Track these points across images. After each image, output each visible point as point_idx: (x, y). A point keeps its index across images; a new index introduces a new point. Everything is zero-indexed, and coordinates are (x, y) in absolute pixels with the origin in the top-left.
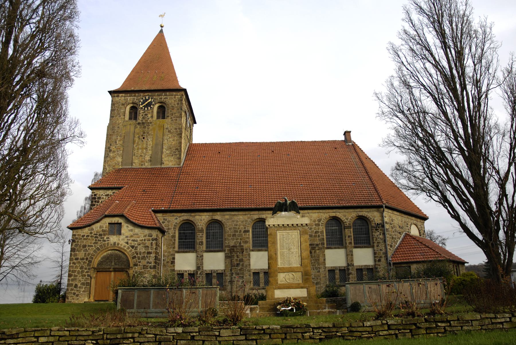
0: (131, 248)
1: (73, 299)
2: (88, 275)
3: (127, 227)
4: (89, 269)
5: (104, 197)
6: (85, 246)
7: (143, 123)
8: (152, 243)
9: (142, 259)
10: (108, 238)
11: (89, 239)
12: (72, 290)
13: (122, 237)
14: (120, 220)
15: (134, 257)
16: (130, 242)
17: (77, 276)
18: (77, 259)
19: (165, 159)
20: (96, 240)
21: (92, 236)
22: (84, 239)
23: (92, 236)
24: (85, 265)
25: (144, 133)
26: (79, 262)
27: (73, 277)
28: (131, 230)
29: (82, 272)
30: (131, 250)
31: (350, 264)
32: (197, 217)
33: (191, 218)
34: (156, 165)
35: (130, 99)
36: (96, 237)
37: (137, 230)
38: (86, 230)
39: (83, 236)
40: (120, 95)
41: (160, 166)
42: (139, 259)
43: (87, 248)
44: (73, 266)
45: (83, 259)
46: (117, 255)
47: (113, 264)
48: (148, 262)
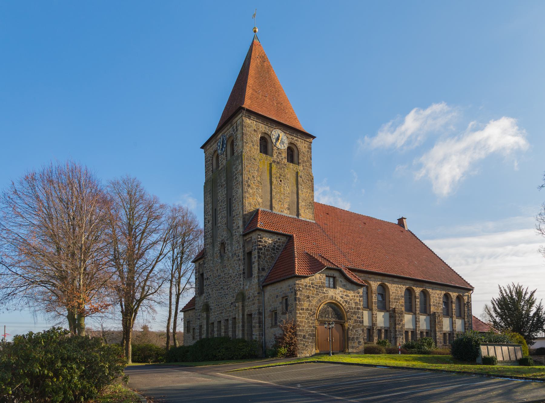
2: (313, 326)
3: (341, 281)
7: (278, 163)
14: (336, 274)
18: (302, 309)
20: (317, 291)
21: (313, 287)
22: (307, 289)
29: (309, 322)
35: (263, 128)
39: (306, 286)
45: (307, 309)
48: (358, 317)
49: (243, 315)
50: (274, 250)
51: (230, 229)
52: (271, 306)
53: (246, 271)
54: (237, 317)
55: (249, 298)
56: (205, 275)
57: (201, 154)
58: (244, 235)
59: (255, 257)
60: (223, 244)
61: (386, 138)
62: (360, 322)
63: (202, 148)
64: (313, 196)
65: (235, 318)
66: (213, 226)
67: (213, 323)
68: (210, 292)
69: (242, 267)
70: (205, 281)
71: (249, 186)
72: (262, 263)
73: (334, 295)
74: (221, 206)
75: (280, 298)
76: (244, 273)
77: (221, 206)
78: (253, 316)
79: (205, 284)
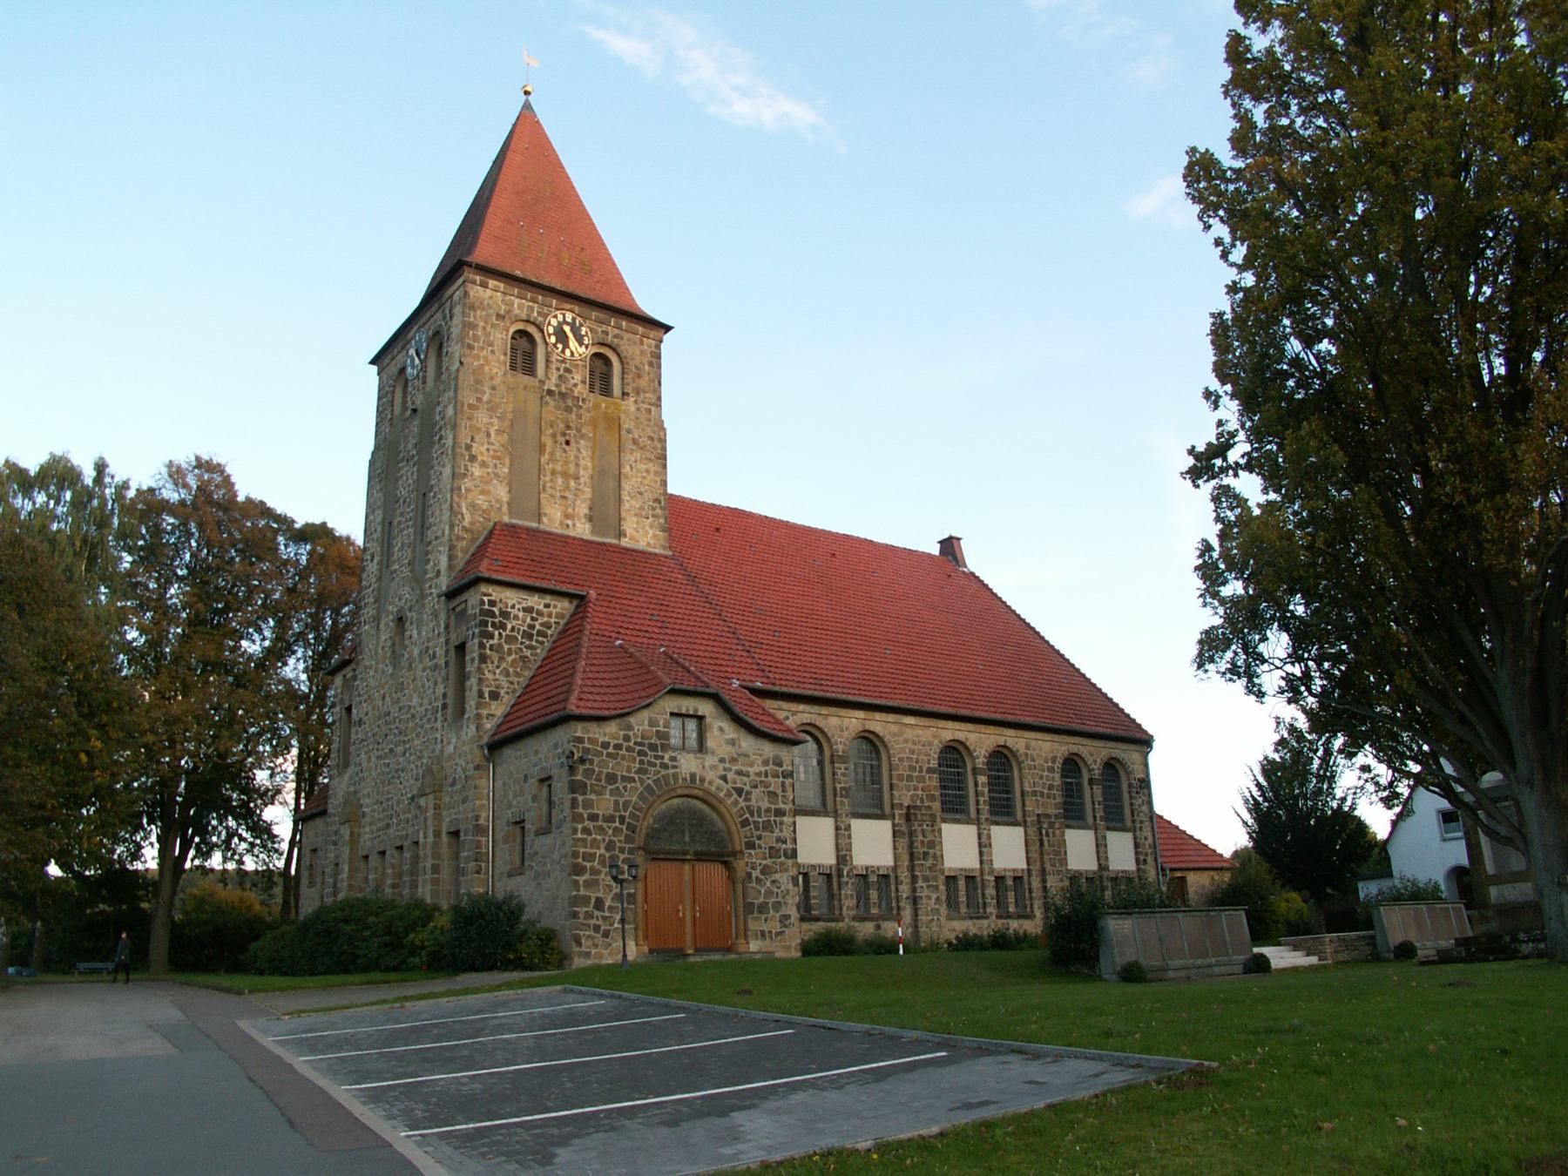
0: (735, 795)
1: (596, 946)
3: (721, 729)
4: (631, 851)
5: (521, 614)
6: (611, 778)
7: (562, 395)
8: (783, 784)
9: (765, 828)
10: (673, 759)
11: (623, 758)
12: (589, 915)
13: (710, 760)
14: (706, 708)
15: (745, 823)
16: (730, 776)
17: (599, 872)
18: (593, 818)
19: (629, 525)
20: (642, 762)
21: (629, 749)
22: (609, 755)
23: (629, 749)
24: (619, 840)
25: (568, 427)
26: (601, 829)
27: (586, 876)
28: (732, 742)
30: (736, 802)
31: (843, 857)
32: (834, 721)
33: (821, 722)
34: (605, 536)
35: (521, 305)
36: (641, 753)
37: (748, 743)
38: (612, 728)
39: (605, 745)
40: (492, 283)
41: (614, 541)
42: (757, 829)
43: (620, 785)
44: (584, 840)
45: (610, 819)
46: (694, 813)
47: (687, 839)
48: (779, 840)
49: (437, 834)
50: (530, 637)
51: (418, 580)
52: (510, 806)
53: (450, 701)
54: (421, 840)
55: (453, 784)
56: (354, 711)
57: (370, 379)
58: (451, 595)
59: (473, 660)
60: (400, 620)
61: (1486, 379)
62: (786, 856)
63: (373, 362)
64: (664, 483)
65: (417, 843)
66: (380, 570)
67: (366, 857)
68: (364, 765)
69: (440, 690)
70: (353, 730)
71: (473, 458)
72: (490, 676)
73: (698, 772)
74: (402, 514)
75: (533, 781)
76: (445, 706)
77: (402, 514)
78: (462, 838)
79: (353, 737)
